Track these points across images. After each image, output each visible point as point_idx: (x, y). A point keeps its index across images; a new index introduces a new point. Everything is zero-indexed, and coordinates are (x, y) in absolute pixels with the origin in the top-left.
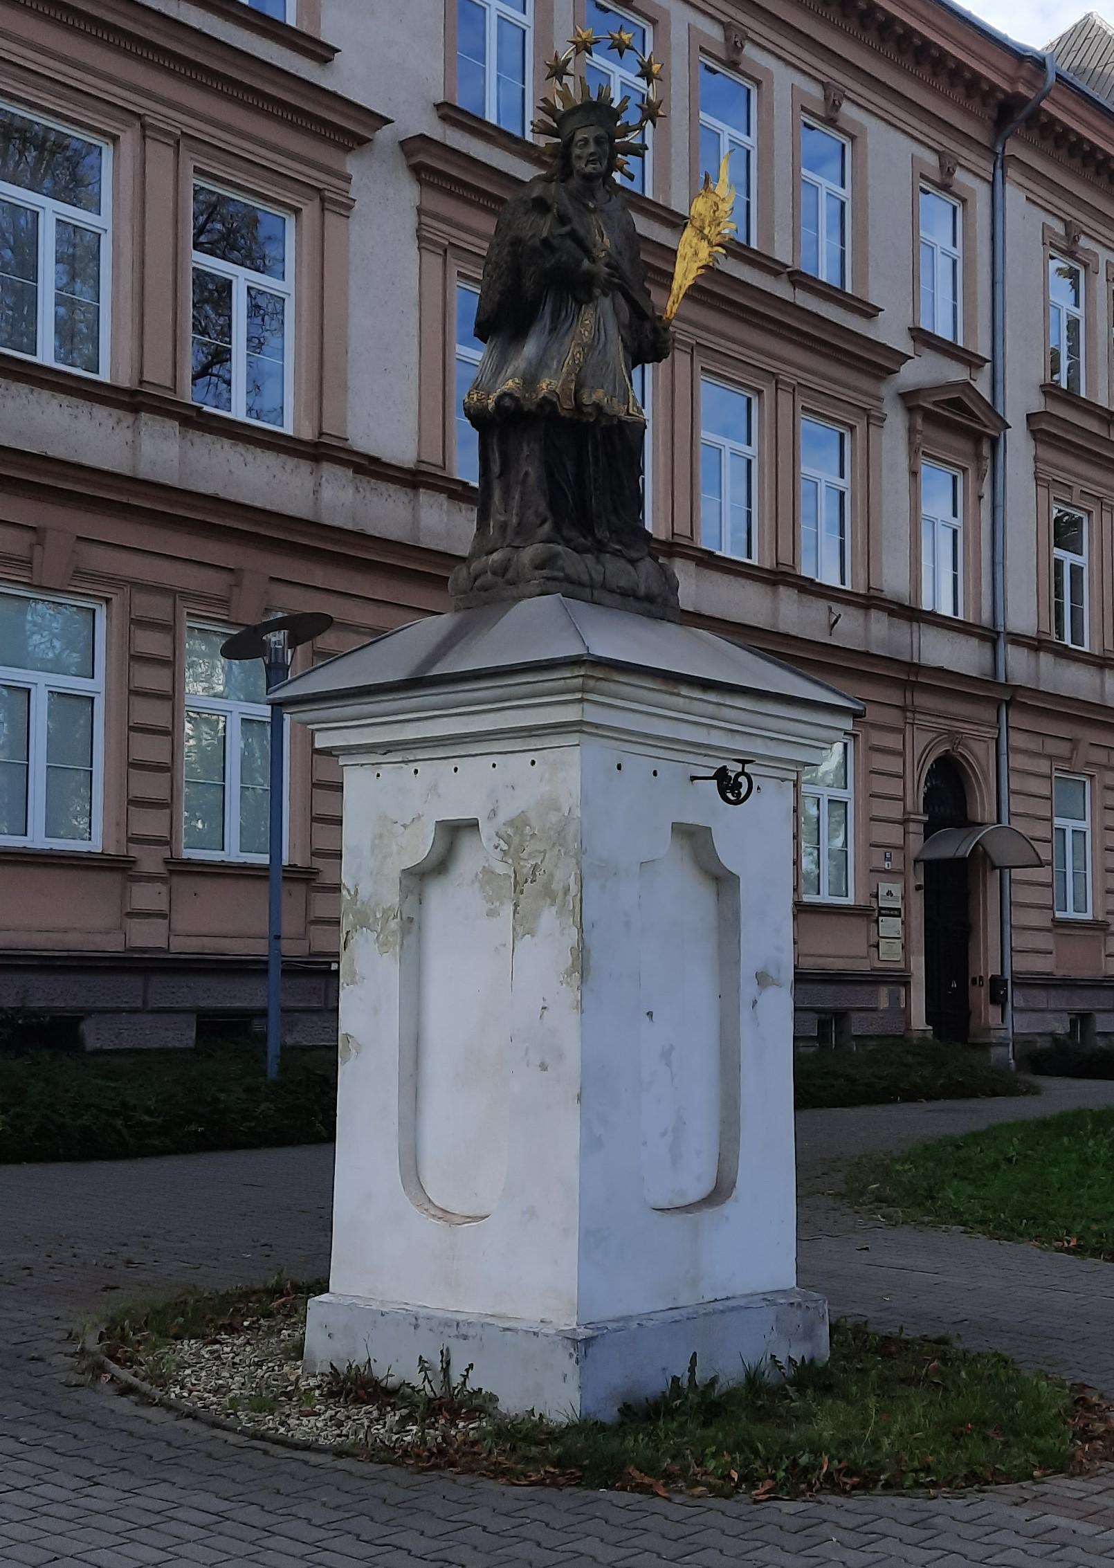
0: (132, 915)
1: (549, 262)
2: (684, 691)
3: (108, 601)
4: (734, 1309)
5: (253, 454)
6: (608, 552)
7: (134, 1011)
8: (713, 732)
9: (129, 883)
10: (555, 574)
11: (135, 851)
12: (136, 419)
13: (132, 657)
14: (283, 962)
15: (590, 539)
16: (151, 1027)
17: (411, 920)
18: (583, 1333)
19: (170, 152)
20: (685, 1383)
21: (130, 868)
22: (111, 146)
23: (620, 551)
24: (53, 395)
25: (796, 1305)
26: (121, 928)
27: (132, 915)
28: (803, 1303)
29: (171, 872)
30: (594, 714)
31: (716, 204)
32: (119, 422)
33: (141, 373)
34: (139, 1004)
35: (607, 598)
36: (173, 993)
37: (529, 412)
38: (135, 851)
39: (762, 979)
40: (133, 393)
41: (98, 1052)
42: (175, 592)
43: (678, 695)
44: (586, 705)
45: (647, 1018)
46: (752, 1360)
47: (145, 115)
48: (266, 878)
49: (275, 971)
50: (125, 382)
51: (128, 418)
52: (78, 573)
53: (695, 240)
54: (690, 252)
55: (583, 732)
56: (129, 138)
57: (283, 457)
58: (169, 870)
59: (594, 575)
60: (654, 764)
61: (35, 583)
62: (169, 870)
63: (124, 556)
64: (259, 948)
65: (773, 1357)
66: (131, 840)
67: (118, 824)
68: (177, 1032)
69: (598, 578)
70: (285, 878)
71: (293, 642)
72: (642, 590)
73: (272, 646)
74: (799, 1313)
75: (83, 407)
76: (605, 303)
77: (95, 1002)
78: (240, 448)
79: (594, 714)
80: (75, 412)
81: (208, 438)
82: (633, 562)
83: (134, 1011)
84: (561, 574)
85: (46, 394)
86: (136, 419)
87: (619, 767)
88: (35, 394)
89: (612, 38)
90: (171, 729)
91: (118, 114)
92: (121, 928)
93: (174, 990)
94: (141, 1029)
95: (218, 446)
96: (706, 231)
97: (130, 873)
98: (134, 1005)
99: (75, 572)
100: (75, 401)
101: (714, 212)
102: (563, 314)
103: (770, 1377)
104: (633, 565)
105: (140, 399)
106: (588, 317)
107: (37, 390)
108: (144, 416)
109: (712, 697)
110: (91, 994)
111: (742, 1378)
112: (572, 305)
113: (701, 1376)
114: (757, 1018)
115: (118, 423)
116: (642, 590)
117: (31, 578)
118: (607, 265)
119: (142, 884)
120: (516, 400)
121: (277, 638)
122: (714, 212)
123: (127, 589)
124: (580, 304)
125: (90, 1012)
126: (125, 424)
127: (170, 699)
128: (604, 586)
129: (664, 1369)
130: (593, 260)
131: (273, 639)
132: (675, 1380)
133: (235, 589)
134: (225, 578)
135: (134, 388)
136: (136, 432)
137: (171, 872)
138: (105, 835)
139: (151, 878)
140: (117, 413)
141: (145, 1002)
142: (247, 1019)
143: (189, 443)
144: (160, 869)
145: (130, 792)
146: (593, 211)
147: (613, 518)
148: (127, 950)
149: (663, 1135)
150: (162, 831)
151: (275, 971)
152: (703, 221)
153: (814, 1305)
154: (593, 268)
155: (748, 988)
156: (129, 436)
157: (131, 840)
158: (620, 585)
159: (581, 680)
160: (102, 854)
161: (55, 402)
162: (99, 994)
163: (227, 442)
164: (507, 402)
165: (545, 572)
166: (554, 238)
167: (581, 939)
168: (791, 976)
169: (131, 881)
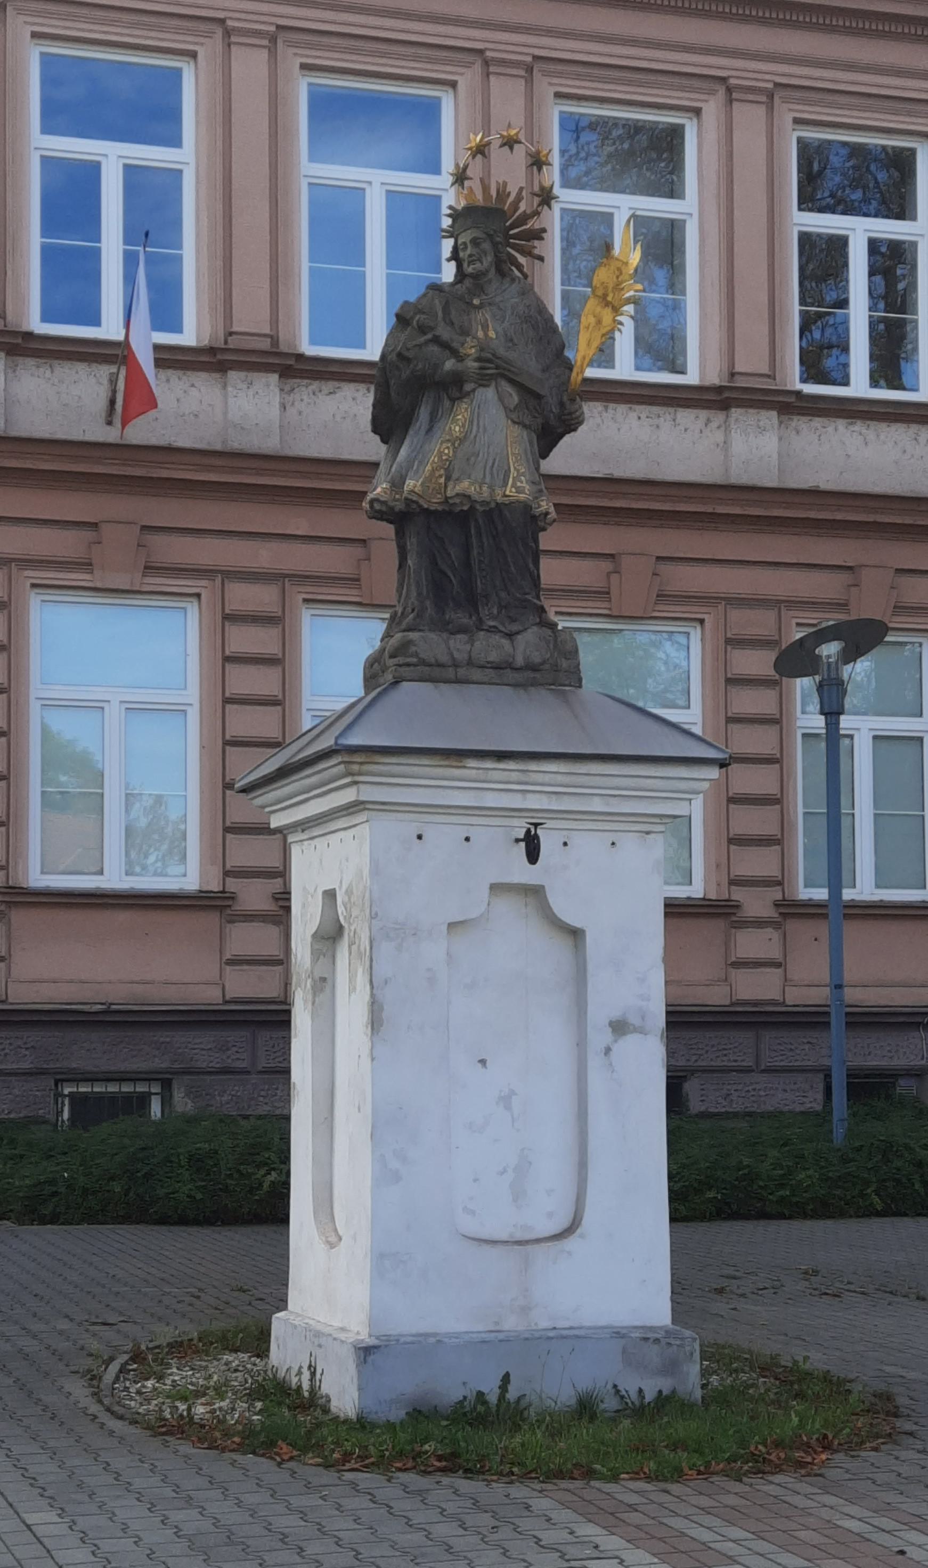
0: (740, 964)
1: (406, 373)
2: (472, 763)
3: (702, 621)
4: (577, 1337)
5: (875, 430)
6: (483, 630)
7: (748, 1070)
8: (529, 796)
9: (734, 930)
10: (409, 660)
11: (738, 894)
12: (727, 416)
13: (729, 681)
14: (847, 1014)
15: (474, 618)
16: (766, 1087)
17: (324, 980)
18: (372, 1342)
19: (761, 111)
20: (493, 1399)
21: (734, 914)
22: (695, 120)
23: (494, 627)
24: (631, 408)
25: (651, 1340)
26: (726, 980)
27: (740, 964)
28: (662, 1340)
29: (784, 915)
30: (368, 793)
31: (619, 269)
32: (708, 421)
33: (732, 363)
34: (749, 1062)
35: (477, 674)
36: (791, 1050)
37: (401, 512)
38: (738, 894)
39: (619, 1027)
40: (719, 389)
41: (704, 1115)
42: (780, 602)
43: (465, 767)
44: (362, 787)
45: (480, 1065)
46: (584, 1385)
47: (729, 77)
48: (825, 916)
49: (838, 1022)
50: (714, 379)
51: (718, 417)
52: (662, 597)
53: (599, 309)
54: (592, 320)
55: (369, 809)
56: (712, 108)
57: (914, 428)
58: (780, 914)
59: (456, 655)
60: (612, 837)
61: (615, 614)
62: (780, 914)
63: (717, 570)
64: (819, 996)
65: (615, 1386)
66: (733, 882)
67: (717, 866)
68: (798, 1094)
69: (460, 656)
70: (845, 915)
71: (851, 654)
72: (520, 661)
73: (825, 661)
74: (655, 1348)
75: (664, 416)
76: (488, 394)
77: (696, 1061)
78: (859, 426)
79: (368, 793)
80: (656, 421)
81: (817, 422)
82: (510, 636)
83: (748, 1070)
84: (415, 660)
85: (622, 408)
86: (727, 416)
87: (420, 837)
88: (610, 411)
89: (502, 136)
90: (778, 756)
91: (696, 83)
92: (726, 980)
93: (793, 1047)
94: (754, 1090)
95: (830, 429)
96: (609, 299)
97: (735, 919)
98: (745, 1064)
99: (658, 596)
100: (656, 409)
101: (618, 277)
102: (440, 413)
103: (610, 1404)
104: (512, 641)
105: (727, 394)
106: (462, 412)
107: (611, 405)
108: (736, 413)
109: (511, 765)
110: (693, 1051)
111: (573, 1402)
112: (447, 403)
113: (512, 1395)
114: (611, 1064)
115: (706, 425)
116: (520, 661)
117: (610, 609)
118: (478, 359)
119: (750, 930)
120: (384, 503)
121: (830, 650)
122: (618, 277)
123: (721, 607)
124: (453, 400)
125: (693, 1071)
126: (714, 425)
127: (777, 723)
128: (470, 663)
129: (464, 1383)
130: (460, 358)
131: (825, 653)
132: (480, 1394)
133: (853, 589)
134: (843, 578)
135: (723, 384)
136: (727, 431)
137: (784, 915)
138: (706, 880)
139: (759, 923)
140: (703, 414)
141: (757, 1063)
142: (892, 1080)
143: (794, 432)
144: (769, 912)
145: (731, 830)
146: (480, 307)
147: (503, 594)
148: (732, 1004)
149: (504, 1171)
150: (773, 871)
151: (838, 1022)
152: (606, 288)
153: (678, 1342)
154: (460, 366)
155: (599, 1037)
156: (719, 436)
157: (733, 882)
158: (489, 659)
159: (342, 766)
160: (704, 899)
161: (633, 415)
162: (703, 1052)
163: (841, 423)
164: (377, 506)
165: (401, 660)
166: (408, 349)
167: (372, 995)
168: (661, 1021)
169: (735, 928)
